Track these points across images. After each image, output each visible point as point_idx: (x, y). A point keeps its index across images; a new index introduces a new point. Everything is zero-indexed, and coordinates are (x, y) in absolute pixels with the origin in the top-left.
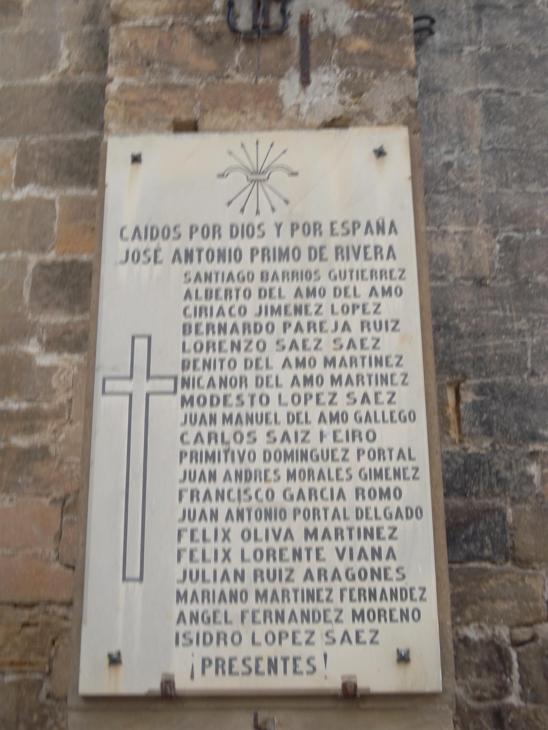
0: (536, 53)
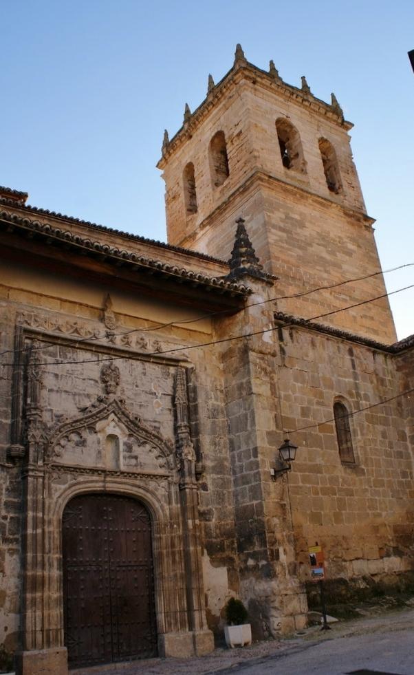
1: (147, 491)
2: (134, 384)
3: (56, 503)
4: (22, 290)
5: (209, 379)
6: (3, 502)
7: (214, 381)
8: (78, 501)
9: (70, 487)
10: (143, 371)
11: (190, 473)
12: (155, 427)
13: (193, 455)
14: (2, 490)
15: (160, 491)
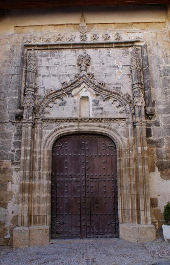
0: (4, 106)
1: (111, 129)
2: (101, 63)
3: (46, 141)
4: (31, 26)
5: (160, 51)
6: (12, 142)
7: (165, 51)
8: (62, 139)
9: (55, 131)
10: (108, 54)
11: (140, 115)
12: (117, 88)
13: (142, 103)
14: (12, 135)
15: (119, 129)
